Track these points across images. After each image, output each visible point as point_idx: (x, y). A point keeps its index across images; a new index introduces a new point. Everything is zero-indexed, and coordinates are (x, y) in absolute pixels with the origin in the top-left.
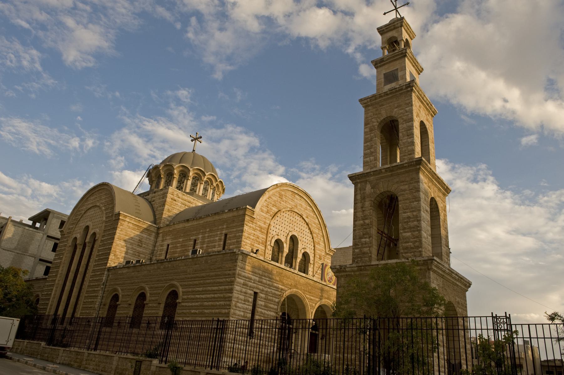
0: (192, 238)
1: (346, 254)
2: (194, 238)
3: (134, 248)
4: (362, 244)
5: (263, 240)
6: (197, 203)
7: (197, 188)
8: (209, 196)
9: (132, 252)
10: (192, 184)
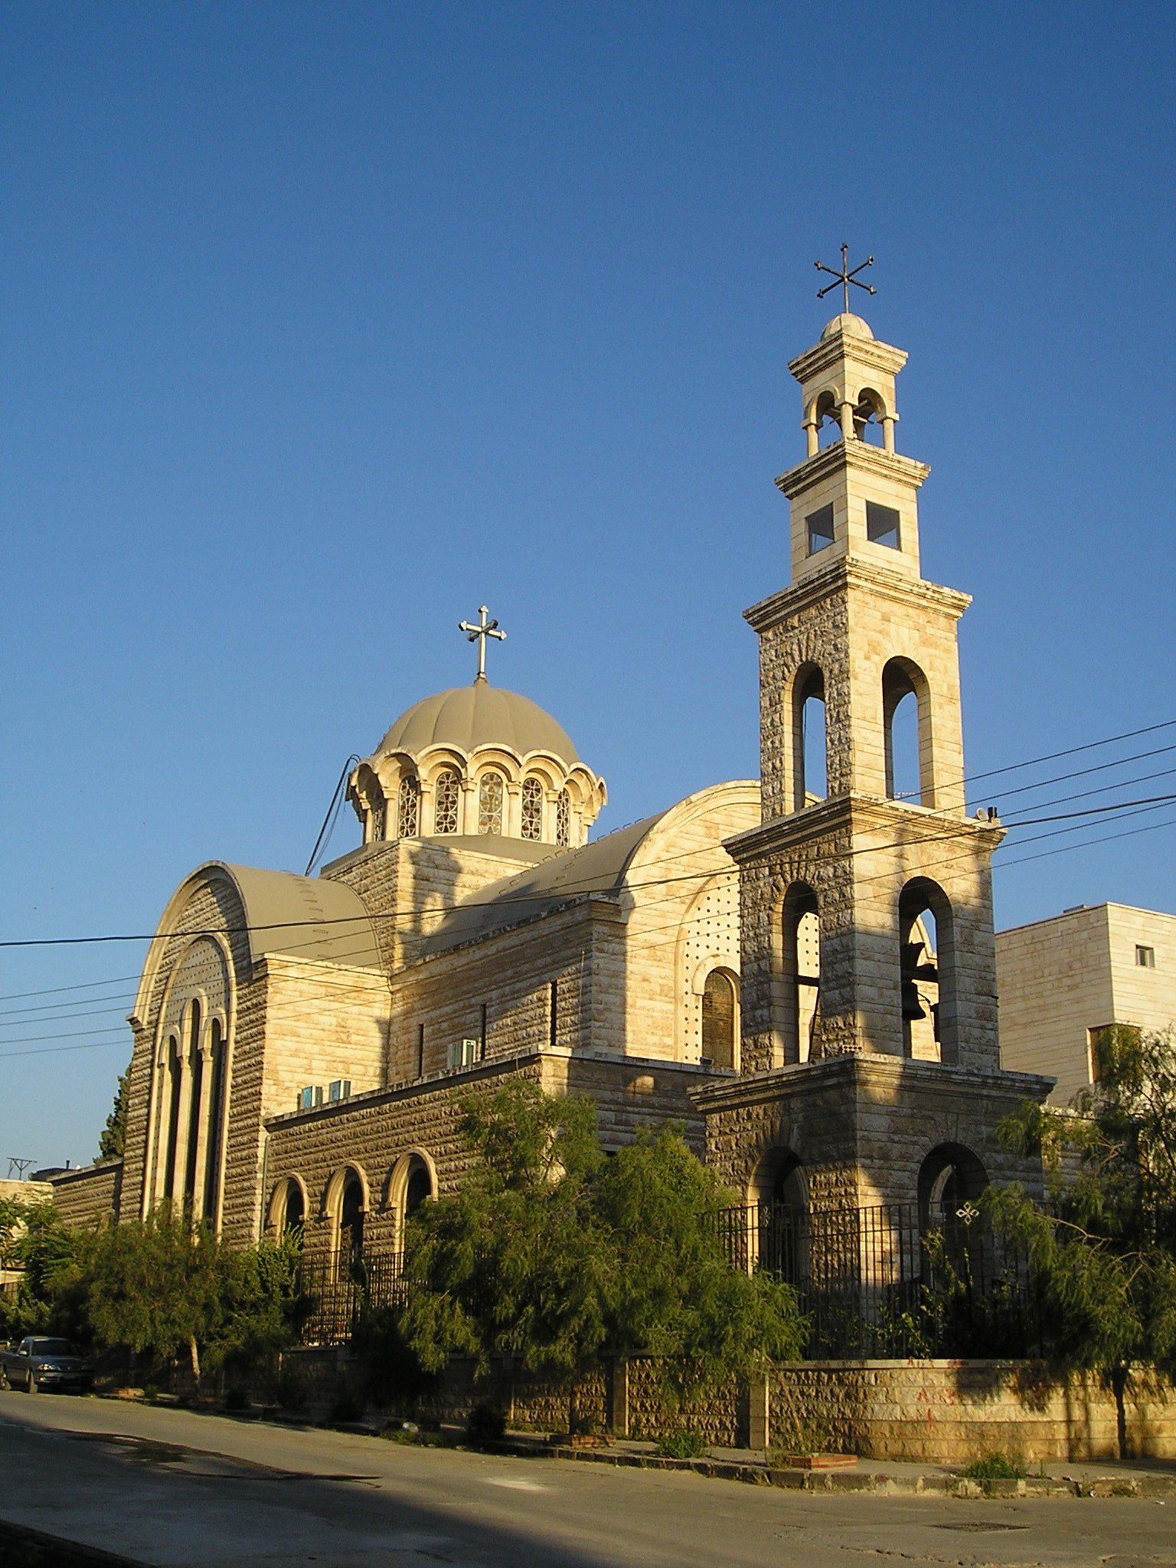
0: (473, 1001)
1: (1039, 946)
2: (479, 999)
3: (329, 1050)
4: (757, 1024)
5: (664, 982)
6: (501, 869)
7: (500, 812)
8: (548, 832)
9: (323, 1065)
10: (483, 802)
